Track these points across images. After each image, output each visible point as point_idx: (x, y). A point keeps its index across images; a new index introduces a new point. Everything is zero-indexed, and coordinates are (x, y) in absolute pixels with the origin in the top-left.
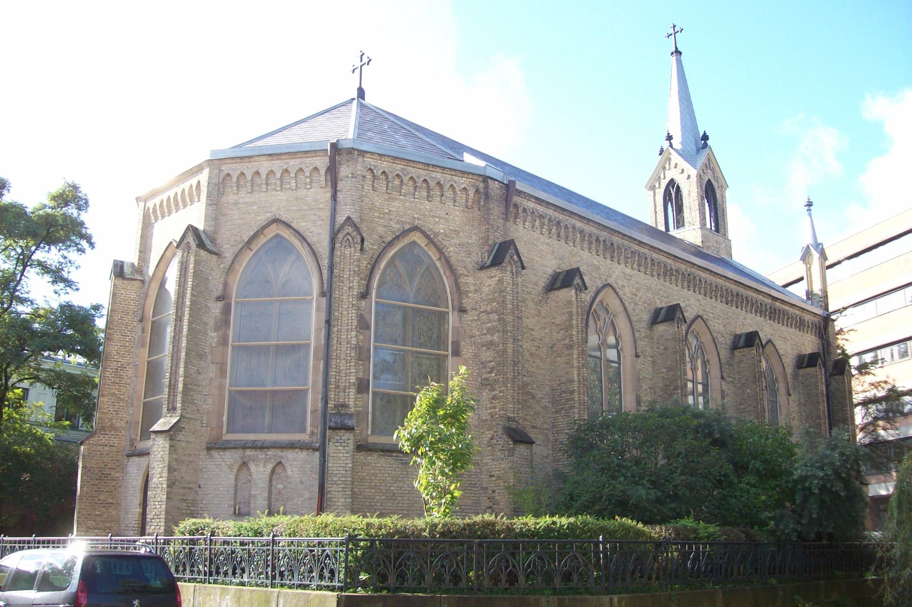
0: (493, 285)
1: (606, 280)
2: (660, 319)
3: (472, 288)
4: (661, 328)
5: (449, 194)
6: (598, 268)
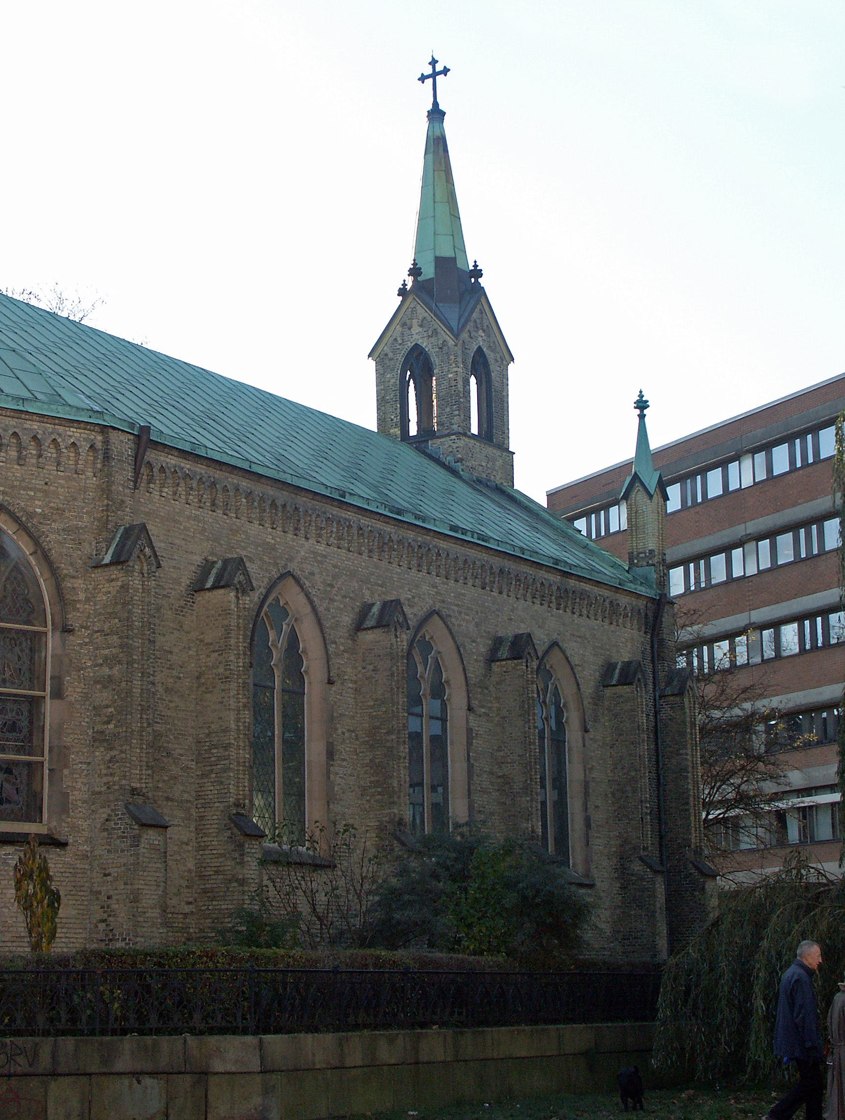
0: (114, 593)
1: (285, 567)
2: (369, 623)
3: (82, 596)
4: (368, 637)
5: (51, 453)
6: (274, 549)
